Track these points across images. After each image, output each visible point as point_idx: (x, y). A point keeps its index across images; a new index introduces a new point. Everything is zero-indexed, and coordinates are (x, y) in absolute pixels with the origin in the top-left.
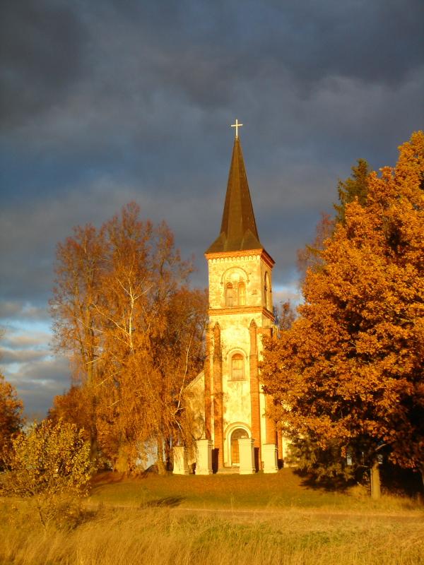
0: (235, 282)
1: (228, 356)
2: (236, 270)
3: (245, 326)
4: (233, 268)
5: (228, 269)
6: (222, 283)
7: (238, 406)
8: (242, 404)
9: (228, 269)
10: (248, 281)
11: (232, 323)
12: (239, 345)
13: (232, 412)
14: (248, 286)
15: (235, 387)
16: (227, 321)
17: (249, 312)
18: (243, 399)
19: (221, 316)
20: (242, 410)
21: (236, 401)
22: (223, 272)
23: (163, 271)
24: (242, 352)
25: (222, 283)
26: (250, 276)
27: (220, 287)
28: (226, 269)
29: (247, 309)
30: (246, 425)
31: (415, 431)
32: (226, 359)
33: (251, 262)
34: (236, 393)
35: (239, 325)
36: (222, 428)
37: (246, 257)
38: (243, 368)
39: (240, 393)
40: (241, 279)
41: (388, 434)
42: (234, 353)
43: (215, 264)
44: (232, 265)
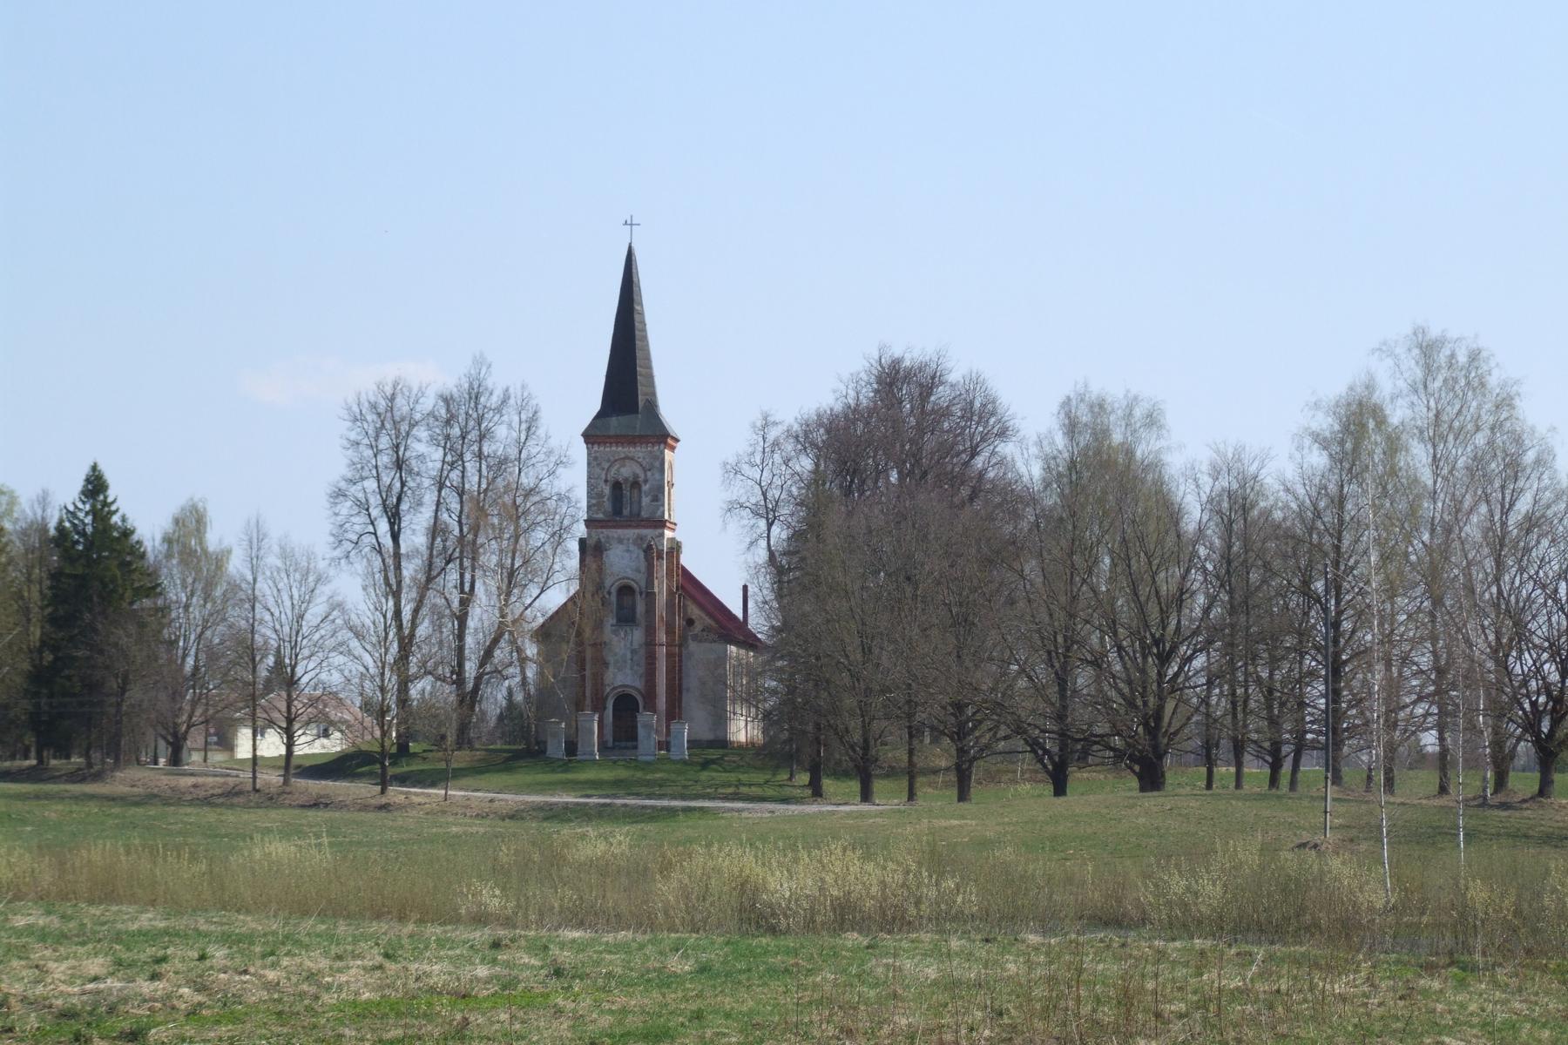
0: (626, 480)
3: (639, 547)
5: (616, 461)
9: (616, 461)
10: (646, 481)
11: (620, 541)
12: (630, 573)
14: (645, 488)
15: (622, 635)
18: (633, 652)
25: (606, 481)
26: (649, 474)
28: (612, 459)
30: (637, 689)
33: (651, 452)
43: (596, 452)
44: (623, 456)
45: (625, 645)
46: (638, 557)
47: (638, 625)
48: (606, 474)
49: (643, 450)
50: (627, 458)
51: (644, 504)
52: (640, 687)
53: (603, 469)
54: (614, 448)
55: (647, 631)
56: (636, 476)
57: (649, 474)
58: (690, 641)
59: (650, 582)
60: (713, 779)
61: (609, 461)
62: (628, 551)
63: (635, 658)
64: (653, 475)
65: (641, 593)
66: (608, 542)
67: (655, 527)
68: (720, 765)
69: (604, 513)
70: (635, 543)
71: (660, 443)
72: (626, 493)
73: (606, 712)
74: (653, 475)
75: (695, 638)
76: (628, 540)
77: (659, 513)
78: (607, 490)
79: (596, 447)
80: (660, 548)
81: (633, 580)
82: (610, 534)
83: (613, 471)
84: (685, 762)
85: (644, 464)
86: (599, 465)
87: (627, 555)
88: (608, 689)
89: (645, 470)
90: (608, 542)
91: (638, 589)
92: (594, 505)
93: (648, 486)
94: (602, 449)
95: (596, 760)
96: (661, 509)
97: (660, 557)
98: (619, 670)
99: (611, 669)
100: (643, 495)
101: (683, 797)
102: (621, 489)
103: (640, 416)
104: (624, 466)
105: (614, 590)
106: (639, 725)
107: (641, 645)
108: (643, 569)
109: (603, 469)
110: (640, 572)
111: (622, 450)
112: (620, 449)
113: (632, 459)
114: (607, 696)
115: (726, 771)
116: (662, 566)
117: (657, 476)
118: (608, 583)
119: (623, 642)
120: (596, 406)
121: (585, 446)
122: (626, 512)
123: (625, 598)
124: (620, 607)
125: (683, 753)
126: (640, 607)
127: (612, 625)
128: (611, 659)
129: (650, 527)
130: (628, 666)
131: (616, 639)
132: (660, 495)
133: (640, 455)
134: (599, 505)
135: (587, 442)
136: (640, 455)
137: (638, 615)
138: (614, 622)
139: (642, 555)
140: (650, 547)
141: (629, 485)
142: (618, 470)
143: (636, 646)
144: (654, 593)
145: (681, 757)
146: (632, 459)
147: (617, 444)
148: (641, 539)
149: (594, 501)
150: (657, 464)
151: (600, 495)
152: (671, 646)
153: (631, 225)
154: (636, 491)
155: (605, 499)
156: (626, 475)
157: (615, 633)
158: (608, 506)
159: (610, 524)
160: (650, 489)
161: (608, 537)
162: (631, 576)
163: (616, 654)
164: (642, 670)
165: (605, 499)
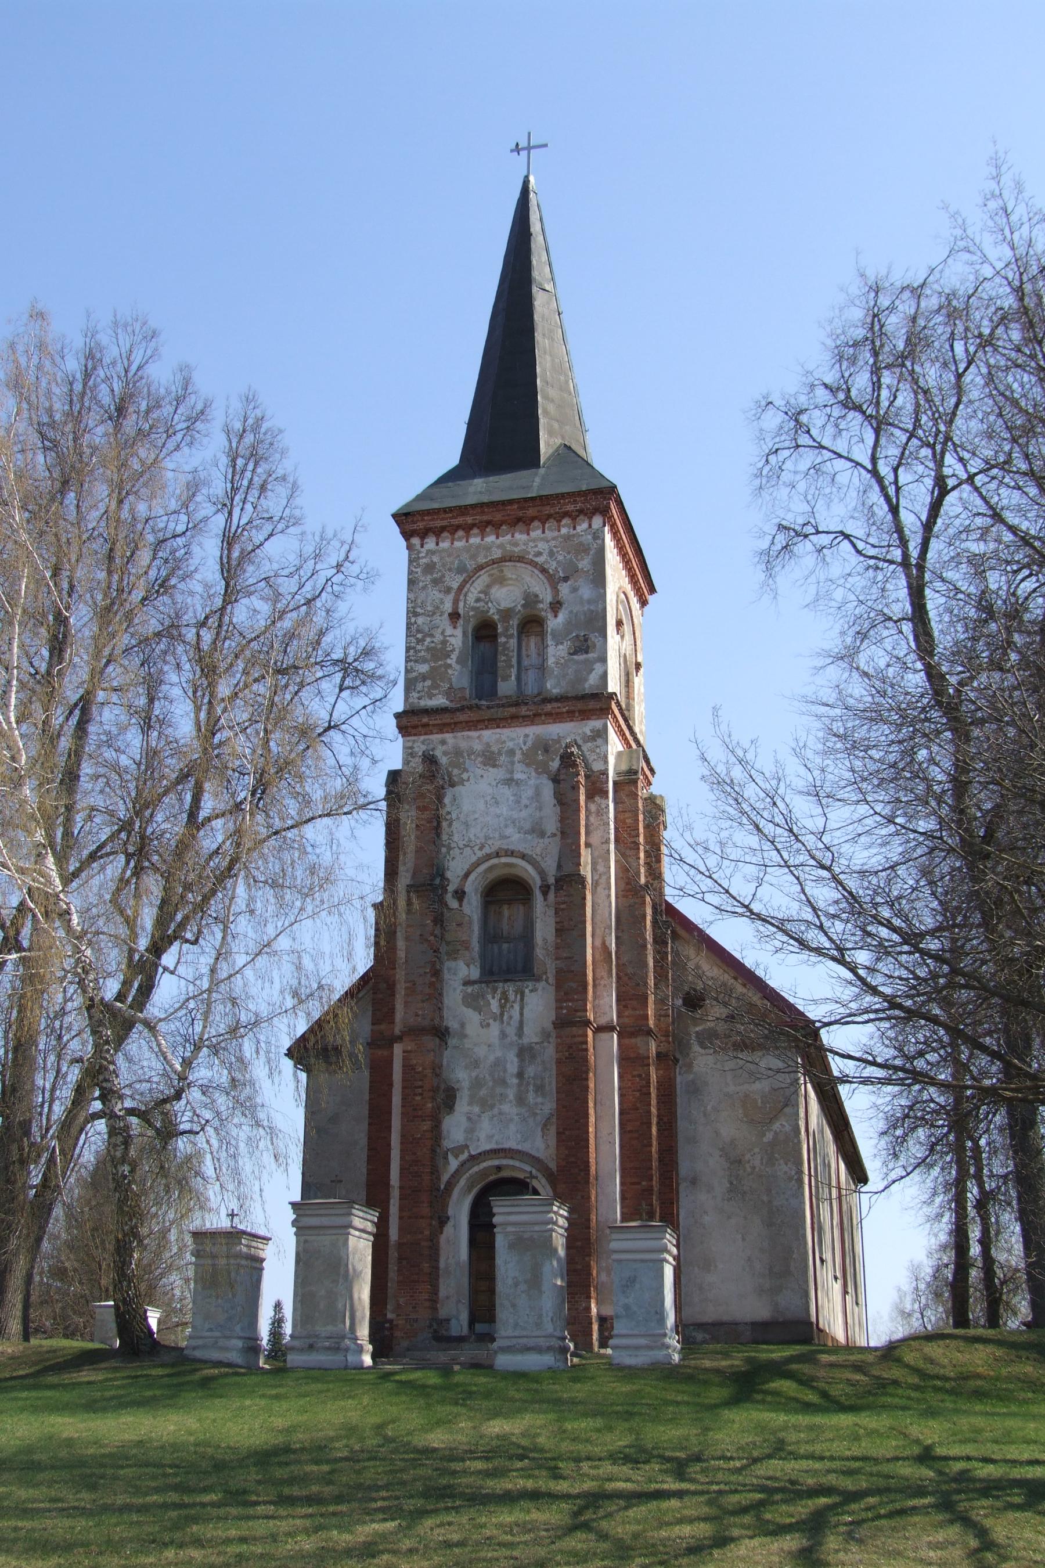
0: (507, 614)
1: (468, 887)
2: (509, 570)
3: (542, 769)
4: (503, 560)
5: (480, 568)
6: (454, 616)
7: (503, 1082)
8: (520, 1075)
9: (480, 568)
10: (556, 606)
11: (490, 759)
12: (516, 840)
13: (476, 1109)
14: (555, 623)
15: (494, 1005)
16: (471, 752)
17: (557, 717)
18: (526, 1053)
19: (448, 737)
20: (521, 1100)
21: (498, 1063)
22: (460, 579)
23: (846, 545)
24: (529, 872)
25: (454, 616)
26: (564, 589)
27: (449, 631)
28: (471, 565)
29: (549, 707)
30: (535, 1161)
31: (586, 680)
32: (460, 895)
33: (568, 538)
34: (495, 1029)
35: (519, 767)
36: (435, 1291)
37: (551, 524)
38: (527, 937)
39: (511, 1031)
40: (530, 600)
41: (966, 1025)
42: (492, 876)
43: (430, 552)
44: (497, 554)
45: (503, 1035)
46: (538, 793)
47: (538, 979)
48: (456, 602)
49: (549, 534)
50: (509, 558)
51: (551, 661)
52: (541, 1155)
53: (448, 590)
54: (475, 540)
55: (558, 987)
56: (530, 600)
57: (564, 589)
58: (696, 1048)
59: (570, 852)
60: (779, 1449)
61: (460, 570)
62: (509, 782)
63: (530, 1071)
64: (575, 590)
65: (545, 890)
66: (458, 765)
67: (585, 715)
68: (805, 1382)
69: (448, 694)
70: (529, 759)
71: (590, 514)
72: (507, 640)
73: (448, 1229)
74: (575, 590)
75: (707, 1039)
76: (511, 753)
77: (593, 679)
78: (457, 638)
79: (430, 543)
80: (597, 767)
81: (523, 857)
82: (463, 745)
83: (474, 592)
84: (668, 1373)
85: (552, 566)
86: (436, 582)
87: (507, 792)
88: (454, 1164)
89: (553, 581)
90: (458, 765)
91: (539, 882)
92: (424, 677)
93: (561, 617)
94: (445, 545)
95: (360, 1367)
96: (598, 668)
97: (596, 790)
98: (486, 1105)
99: (462, 1106)
100: (550, 642)
101: (800, 1182)
102: (493, 637)
103: (542, 471)
104: (501, 581)
105: (473, 887)
106: (500, 1241)
107: (546, 1035)
108: (551, 825)
109: (448, 590)
110: (542, 834)
111: (494, 543)
112: (491, 539)
113: (520, 559)
114: (450, 1185)
115: (833, 1405)
116: (602, 812)
117: (586, 592)
118: (455, 868)
119: (495, 1029)
120: (453, 459)
121: (403, 543)
122: (506, 687)
123: (506, 911)
124: (490, 937)
125: (657, 1340)
126: (544, 930)
127: (467, 983)
128: (461, 1076)
129: (571, 716)
130: (511, 1094)
131: (473, 1017)
132: (594, 637)
133: (542, 546)
134: (435, 676)
135: (407, 535)
136: (542, 546)
137: (539, 952)
138: (475, 973)
139: (548, 790)
140: (568, 760)
141: (515, 622)
142: (486, 591)
143: (531, 1035)
144: (582, 880)
145: (659, 1355)
146: (520, 559)
147: (483, 527)
148: (546, 750)
149: (423, 668)
150: (585, 564)
151: (440, 653)
152: (633, 1035)
153: (529, 148)
154: (533, 642)
155: (452, 661)
156: (505, 605)
157: (473, 1002)
158: (459, 675)
159: (462, 717)
160: (569, 624)
161: (458, 753)
162: (521, 848)
163: (476, 1064)
164: (548, 1106)
165: (452, 661)
